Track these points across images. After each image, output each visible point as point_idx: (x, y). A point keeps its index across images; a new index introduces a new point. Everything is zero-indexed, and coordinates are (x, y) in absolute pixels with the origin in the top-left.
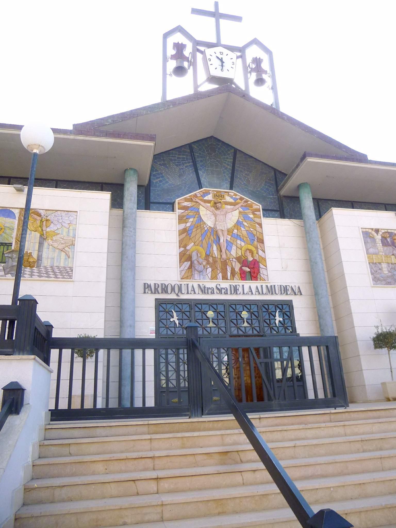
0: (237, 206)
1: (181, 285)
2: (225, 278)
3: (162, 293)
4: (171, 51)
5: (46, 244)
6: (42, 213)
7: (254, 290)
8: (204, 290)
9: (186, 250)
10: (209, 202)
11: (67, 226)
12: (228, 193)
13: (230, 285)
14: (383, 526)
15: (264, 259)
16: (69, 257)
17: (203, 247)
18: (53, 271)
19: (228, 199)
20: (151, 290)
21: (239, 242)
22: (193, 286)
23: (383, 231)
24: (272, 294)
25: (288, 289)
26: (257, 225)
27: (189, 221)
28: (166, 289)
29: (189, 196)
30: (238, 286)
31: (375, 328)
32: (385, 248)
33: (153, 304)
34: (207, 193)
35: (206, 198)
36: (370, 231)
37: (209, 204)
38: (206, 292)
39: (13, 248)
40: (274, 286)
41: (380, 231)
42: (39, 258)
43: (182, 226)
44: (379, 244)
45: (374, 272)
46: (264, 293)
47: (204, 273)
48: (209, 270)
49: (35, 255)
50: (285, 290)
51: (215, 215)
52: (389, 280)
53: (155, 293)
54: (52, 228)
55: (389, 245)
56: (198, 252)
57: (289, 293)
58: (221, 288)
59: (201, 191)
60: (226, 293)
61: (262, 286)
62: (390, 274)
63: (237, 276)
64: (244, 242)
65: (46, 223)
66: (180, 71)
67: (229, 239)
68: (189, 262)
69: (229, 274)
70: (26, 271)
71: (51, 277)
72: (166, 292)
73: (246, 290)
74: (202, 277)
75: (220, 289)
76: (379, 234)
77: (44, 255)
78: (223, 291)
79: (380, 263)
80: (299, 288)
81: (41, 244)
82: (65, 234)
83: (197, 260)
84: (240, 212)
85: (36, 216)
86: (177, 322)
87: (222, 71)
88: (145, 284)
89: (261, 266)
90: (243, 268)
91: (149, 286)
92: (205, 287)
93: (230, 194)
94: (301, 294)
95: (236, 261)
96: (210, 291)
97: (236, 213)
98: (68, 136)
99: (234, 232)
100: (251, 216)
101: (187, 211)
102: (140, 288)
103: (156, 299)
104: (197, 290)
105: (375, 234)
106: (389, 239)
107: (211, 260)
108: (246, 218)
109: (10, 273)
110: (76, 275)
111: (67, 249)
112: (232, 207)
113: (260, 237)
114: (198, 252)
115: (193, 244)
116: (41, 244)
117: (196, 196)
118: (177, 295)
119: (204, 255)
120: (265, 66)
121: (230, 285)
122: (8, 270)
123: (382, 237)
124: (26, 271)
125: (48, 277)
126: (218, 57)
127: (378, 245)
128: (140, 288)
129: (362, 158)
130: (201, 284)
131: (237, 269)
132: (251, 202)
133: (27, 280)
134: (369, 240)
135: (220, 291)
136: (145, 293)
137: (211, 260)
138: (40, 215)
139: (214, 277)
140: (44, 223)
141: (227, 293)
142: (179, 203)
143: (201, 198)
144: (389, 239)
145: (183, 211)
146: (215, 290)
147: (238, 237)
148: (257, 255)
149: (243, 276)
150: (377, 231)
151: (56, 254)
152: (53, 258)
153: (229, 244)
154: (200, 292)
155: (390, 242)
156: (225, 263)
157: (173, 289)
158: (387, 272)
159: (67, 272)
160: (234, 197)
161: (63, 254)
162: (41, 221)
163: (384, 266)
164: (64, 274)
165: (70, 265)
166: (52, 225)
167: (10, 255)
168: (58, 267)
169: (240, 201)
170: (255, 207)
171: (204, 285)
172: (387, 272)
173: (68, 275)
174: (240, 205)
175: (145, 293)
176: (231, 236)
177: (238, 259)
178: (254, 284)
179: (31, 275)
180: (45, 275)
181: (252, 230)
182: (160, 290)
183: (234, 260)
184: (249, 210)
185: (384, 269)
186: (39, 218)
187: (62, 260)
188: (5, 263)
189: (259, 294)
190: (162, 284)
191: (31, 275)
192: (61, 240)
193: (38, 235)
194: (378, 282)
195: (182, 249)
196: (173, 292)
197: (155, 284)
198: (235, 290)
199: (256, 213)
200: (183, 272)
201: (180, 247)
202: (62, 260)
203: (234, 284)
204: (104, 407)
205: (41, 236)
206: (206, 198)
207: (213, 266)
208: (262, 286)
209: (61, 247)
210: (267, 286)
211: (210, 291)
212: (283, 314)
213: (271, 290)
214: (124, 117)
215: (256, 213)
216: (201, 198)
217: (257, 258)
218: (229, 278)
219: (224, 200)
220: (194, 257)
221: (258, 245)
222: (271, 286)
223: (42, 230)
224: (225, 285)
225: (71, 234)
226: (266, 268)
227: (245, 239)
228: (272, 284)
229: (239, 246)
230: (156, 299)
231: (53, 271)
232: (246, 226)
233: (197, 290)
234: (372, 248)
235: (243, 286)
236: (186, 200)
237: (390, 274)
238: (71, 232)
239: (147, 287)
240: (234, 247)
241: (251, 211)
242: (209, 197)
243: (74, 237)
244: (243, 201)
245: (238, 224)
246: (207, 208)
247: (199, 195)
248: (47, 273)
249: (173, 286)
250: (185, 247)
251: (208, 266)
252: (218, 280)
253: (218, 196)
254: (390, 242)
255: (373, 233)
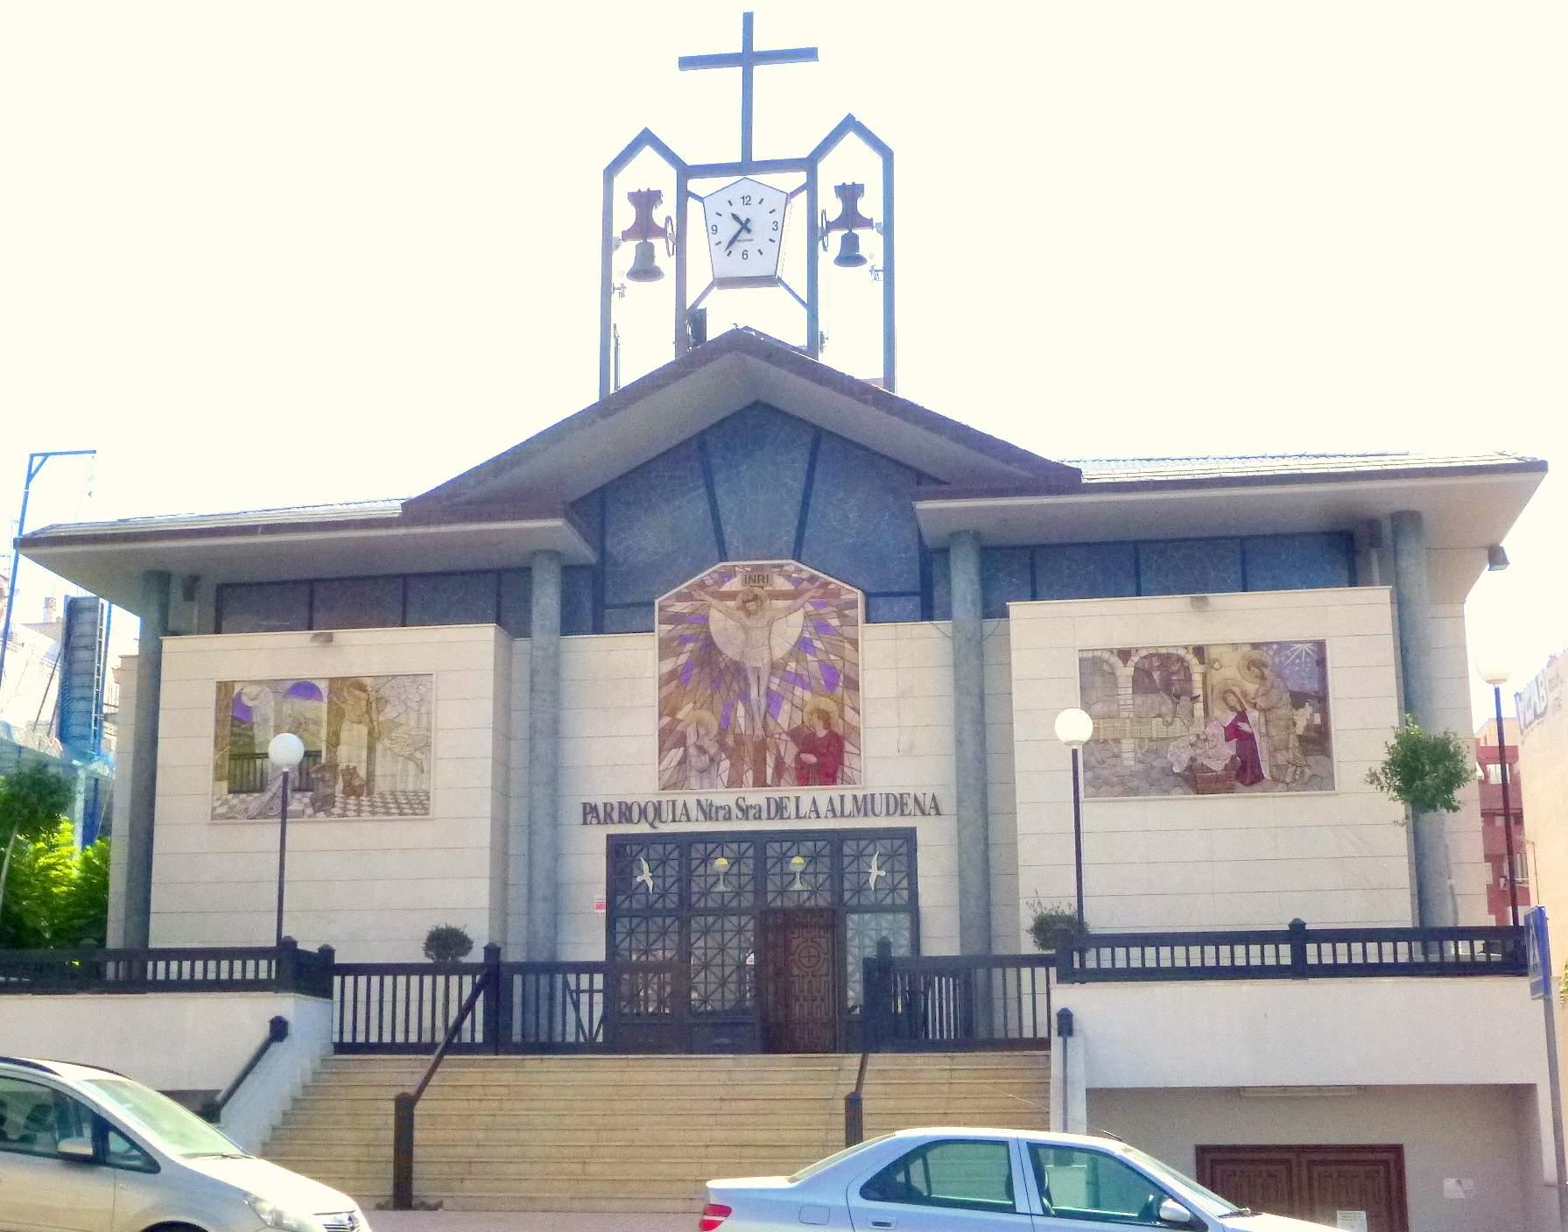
0: (800, 601)
1: (660, 803)
2: (760, 782)
3: (620, 822)
4: (625, 215)
5: (379, 748)
6: (368, 682)
7: (823, 807)
8: (708, 812)
9: (676, 721)
10: (732, 596)
11: (415, 706)
12: (781, 566)
13: (768, 799)
14: (604, 1198)
15: (856, 730)
16: (423, 772)
17: (713, 710)
18: (396, 801)
19: (781, 584)
20: (598, 816)
21: (798, 691)
22: (685, 804)
23: (1144, 653)
24: (866, 815)
25: (905, 801)
26: (847, 645)
27: (685, 651)
28: (627, 813)
29: (687, 588)
30: (785, 800)
31: (1027, 907)
32: (1139, 700)
33: (601, 847)
34: (728, 575)
35: (726, 587)
36: (1106, 655)
37: (733, 603)
38: (713, 815)
39: (323, 761)
40: (873, 795)
41: (1133, 652)
42: (371, 774)
43: (669, 665)
44: (1126, 689)
45: (1096, 764)
46: (847, 812)
47: (714, 773)
48: (725, 764)
49: (362, 772)
50: (898, 804)
51: (745, 629)
52: (1135, 783)
53: (606, 822)
54: (390, 712)
55: (1156, 691)
56: (699, 723)
57: (907, 812)
58: (747, 807)
59: (714, 572)
60: (758, 817)
61: (842, 797)
62: (1140, 767)
63: (789, 776)
64: (811, 690)
65: (377, 704)
66: (645, 270)
67: (774, 687)
68: (682, 749)
69: (769, 771)
70: (349, 804)
71: (393, 814)
72: (629, 820)
73: (805, 807)
74: (706, 782)
75: (745, 807)
76: (1130, 663)
77: (378, 771)
78: (752, 812)
79: (1117, 741)
80: (934, 798)
81: (371, 750)
82: (412, 724)
83: (698, 743)
84: (807, 616)
85: (357, 692)
86: (650, 883)
87: (745, 257)
88: (585, 804)
89: (848, 747)
90: (803, 756)
91: (594, 809)
92: (711, 805)
93: (786, 568)
94: (938, 813)
95: (788, 739)
96: (721, 814)
97: (797, 618)
98: (395, 531)
99: (788, 668)
100: (835, 622)
101: (679, 627)
102: (574, 814)
103: (609, 837)
104: (694, 811)
105: (1120, 663)
106: (1158, 673)
107: (730, 741)
108: (822, 627)
109: (324, 808)
110: (437, 806)
111: (418, 755)
112: (788, 602)
113: (852, 675)
114: (699, 723)
115: (691, 705)
116: (371, 750)
117: (702, 585)
118: (652, 825)
119: (715, 730)
120: (870, 206)
121: (768, 799)
122: (319, 804)
123: (1136, 669)
124: (349, 804)
125: (388, 813)
126: (735, 217)
127: (1121, 691)
128: (574, 814)
129: (1064, 479)
130: (702, 798)
131: (789, 760)
132: (838, 585)
133: (353, 821)
134: (1098, 680)
135: (745, 811)
136: (585, 823)
137: (730, 741)
138: (362, 688)
139: (735, 781)
140: (374, 705)
141: (760, 818)
142: (661, 609)
143: (716, 587)
144: (1158, 673)
145: (670, 627)
146: (735, 811)
147: (797, 679)
148: (840, 721)
149: (805, 777)
150: (1125, 654)
151: (400, 766)
152: (393, 776)
153: (774, 701)
154: (701, 817)
155: (1157, 682)
156: (761, 748)
157: (643, 812)
158: (1132, 763)
159: (421, 803)
160: (794, 575)
161: (411, 765)
162: (369, 703)
163: (1128, 745)
164: (415, 806)
165: (424, 787)
166: (389, 708)
167: (319, 776)
168: (404, 792)
169: (810, 586)
170: (846, 597)
171: (709, 802)
172: (1132, 763)
173: (423, 808)
174: (806, 597)
175: (585, 823)
176: (781, 678)
177: (794, 734)
178: (822, 794)
179: (359, 812)
180: (382, 810)
181: (832, 657)
182: (615, 816)
183: (784, 737)
184: (830, 605)
185: (1126, 755)
186: (363, 695)
187: (411, 779)
188: (312, 790)
189: (835, 816)
190: (620, 803)
191: (359, 812)
192: (406, 736)
193: (364, 730)
194: (1103, 789)
195: (666, 720)
196: (643, 820)
197: (605, 804)
198: (780, 809)
199: (847, 612)
200: (668, 773)
201: (661, 716)
202: (411, 779)
203: (777, 795)
204: (1417, 925)
205: (370, 733)
206: (726, 587)
207: (735, 755)
208: (842, 797)
209: (407, 751)
210: (855, 797)
211: (721, 814)
212: (888, 858)
213: (865, 805)
214: (499, 464)
215: (847, 612)
216: (716, 587)
217: (839, 729)
218: (769, 781)
219: (768, 588)
220: (691, 739)
221: (846, 697)
222: (865, 796)
223: (371, 721)
224: (756, 797)
225: (424, 723)
226: (857, 752)
227: (814, 683)
228: (868, 792)
229: (798, 702)
230: (609, 837)
231: (396, 801)
232: (819, 649)
233: (694, 811)
234: (1103, 701)
235: (798, 798)
236: (680, 597)
237: (1140, 767)
238: (424, 718)
239: (589, 811)
240: (786, 707)
241: (835, 609)
242: (734, 585)
243: (429, 730)
244: (818, 583)
245: (803, 645)
246: (727, 613)
247: (709, 582)
248: (385, 804)
249: (642, 807)
250: (673, 713)
251: (724, 756)
252: (744, 789)
253: (757, 577)
254: (1157, 682)
255: (1115, 660)
